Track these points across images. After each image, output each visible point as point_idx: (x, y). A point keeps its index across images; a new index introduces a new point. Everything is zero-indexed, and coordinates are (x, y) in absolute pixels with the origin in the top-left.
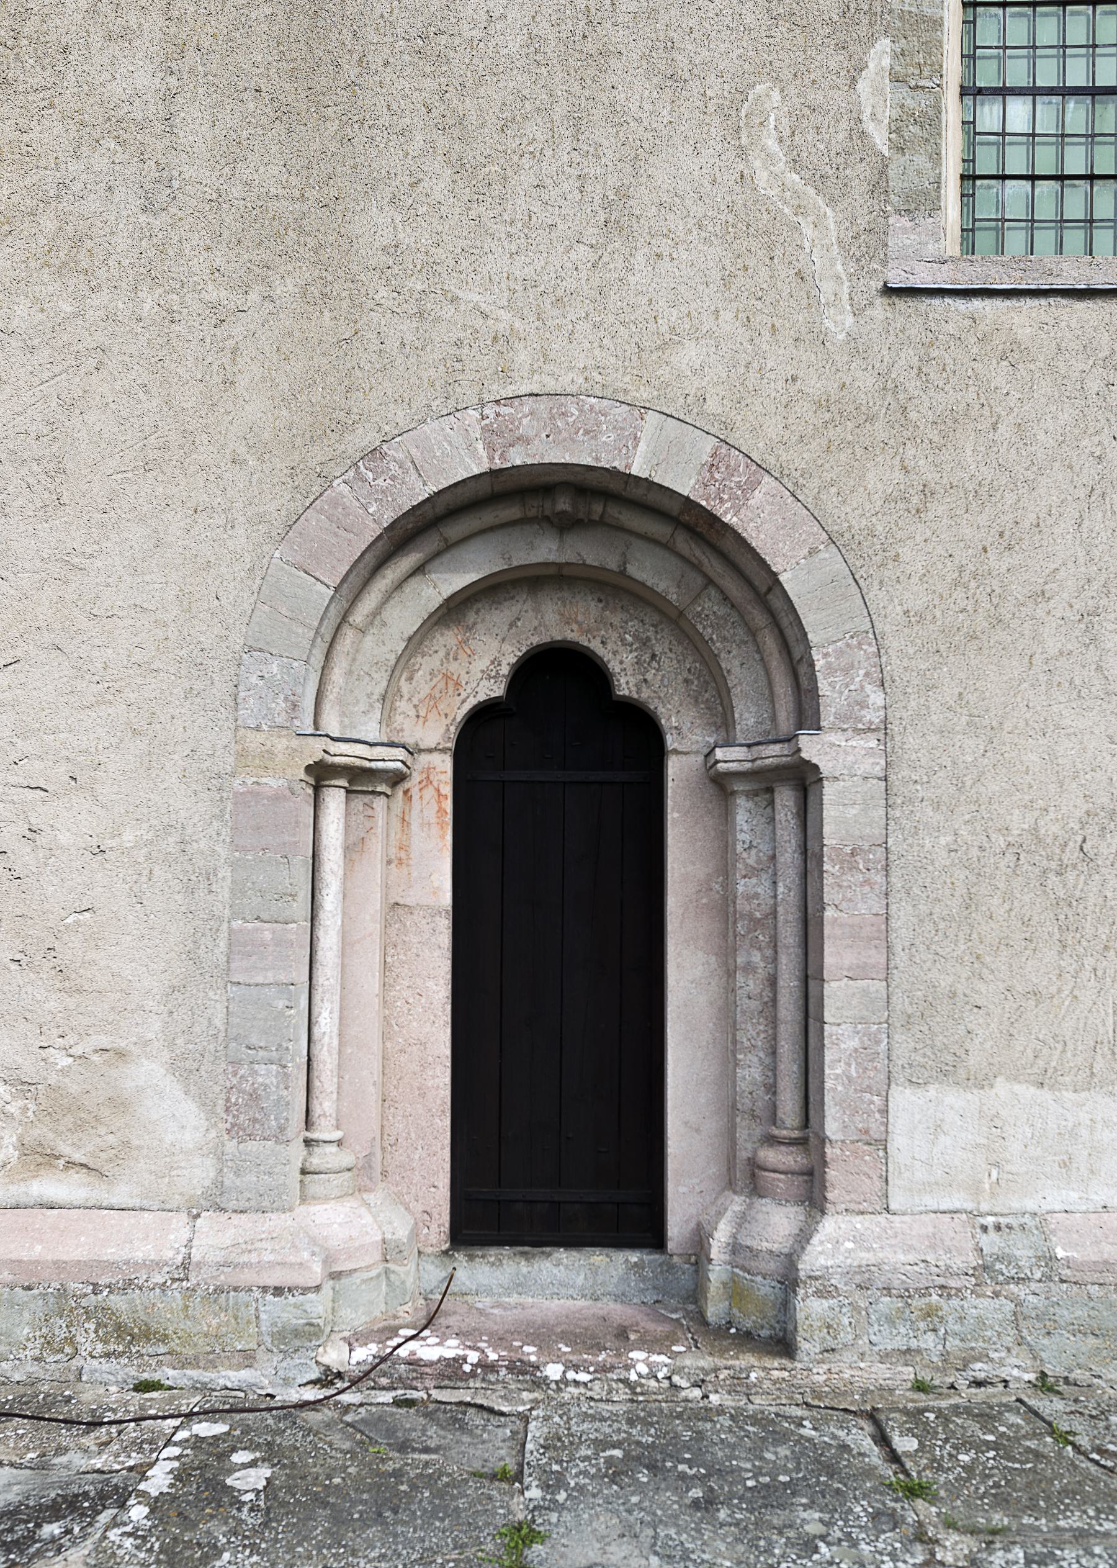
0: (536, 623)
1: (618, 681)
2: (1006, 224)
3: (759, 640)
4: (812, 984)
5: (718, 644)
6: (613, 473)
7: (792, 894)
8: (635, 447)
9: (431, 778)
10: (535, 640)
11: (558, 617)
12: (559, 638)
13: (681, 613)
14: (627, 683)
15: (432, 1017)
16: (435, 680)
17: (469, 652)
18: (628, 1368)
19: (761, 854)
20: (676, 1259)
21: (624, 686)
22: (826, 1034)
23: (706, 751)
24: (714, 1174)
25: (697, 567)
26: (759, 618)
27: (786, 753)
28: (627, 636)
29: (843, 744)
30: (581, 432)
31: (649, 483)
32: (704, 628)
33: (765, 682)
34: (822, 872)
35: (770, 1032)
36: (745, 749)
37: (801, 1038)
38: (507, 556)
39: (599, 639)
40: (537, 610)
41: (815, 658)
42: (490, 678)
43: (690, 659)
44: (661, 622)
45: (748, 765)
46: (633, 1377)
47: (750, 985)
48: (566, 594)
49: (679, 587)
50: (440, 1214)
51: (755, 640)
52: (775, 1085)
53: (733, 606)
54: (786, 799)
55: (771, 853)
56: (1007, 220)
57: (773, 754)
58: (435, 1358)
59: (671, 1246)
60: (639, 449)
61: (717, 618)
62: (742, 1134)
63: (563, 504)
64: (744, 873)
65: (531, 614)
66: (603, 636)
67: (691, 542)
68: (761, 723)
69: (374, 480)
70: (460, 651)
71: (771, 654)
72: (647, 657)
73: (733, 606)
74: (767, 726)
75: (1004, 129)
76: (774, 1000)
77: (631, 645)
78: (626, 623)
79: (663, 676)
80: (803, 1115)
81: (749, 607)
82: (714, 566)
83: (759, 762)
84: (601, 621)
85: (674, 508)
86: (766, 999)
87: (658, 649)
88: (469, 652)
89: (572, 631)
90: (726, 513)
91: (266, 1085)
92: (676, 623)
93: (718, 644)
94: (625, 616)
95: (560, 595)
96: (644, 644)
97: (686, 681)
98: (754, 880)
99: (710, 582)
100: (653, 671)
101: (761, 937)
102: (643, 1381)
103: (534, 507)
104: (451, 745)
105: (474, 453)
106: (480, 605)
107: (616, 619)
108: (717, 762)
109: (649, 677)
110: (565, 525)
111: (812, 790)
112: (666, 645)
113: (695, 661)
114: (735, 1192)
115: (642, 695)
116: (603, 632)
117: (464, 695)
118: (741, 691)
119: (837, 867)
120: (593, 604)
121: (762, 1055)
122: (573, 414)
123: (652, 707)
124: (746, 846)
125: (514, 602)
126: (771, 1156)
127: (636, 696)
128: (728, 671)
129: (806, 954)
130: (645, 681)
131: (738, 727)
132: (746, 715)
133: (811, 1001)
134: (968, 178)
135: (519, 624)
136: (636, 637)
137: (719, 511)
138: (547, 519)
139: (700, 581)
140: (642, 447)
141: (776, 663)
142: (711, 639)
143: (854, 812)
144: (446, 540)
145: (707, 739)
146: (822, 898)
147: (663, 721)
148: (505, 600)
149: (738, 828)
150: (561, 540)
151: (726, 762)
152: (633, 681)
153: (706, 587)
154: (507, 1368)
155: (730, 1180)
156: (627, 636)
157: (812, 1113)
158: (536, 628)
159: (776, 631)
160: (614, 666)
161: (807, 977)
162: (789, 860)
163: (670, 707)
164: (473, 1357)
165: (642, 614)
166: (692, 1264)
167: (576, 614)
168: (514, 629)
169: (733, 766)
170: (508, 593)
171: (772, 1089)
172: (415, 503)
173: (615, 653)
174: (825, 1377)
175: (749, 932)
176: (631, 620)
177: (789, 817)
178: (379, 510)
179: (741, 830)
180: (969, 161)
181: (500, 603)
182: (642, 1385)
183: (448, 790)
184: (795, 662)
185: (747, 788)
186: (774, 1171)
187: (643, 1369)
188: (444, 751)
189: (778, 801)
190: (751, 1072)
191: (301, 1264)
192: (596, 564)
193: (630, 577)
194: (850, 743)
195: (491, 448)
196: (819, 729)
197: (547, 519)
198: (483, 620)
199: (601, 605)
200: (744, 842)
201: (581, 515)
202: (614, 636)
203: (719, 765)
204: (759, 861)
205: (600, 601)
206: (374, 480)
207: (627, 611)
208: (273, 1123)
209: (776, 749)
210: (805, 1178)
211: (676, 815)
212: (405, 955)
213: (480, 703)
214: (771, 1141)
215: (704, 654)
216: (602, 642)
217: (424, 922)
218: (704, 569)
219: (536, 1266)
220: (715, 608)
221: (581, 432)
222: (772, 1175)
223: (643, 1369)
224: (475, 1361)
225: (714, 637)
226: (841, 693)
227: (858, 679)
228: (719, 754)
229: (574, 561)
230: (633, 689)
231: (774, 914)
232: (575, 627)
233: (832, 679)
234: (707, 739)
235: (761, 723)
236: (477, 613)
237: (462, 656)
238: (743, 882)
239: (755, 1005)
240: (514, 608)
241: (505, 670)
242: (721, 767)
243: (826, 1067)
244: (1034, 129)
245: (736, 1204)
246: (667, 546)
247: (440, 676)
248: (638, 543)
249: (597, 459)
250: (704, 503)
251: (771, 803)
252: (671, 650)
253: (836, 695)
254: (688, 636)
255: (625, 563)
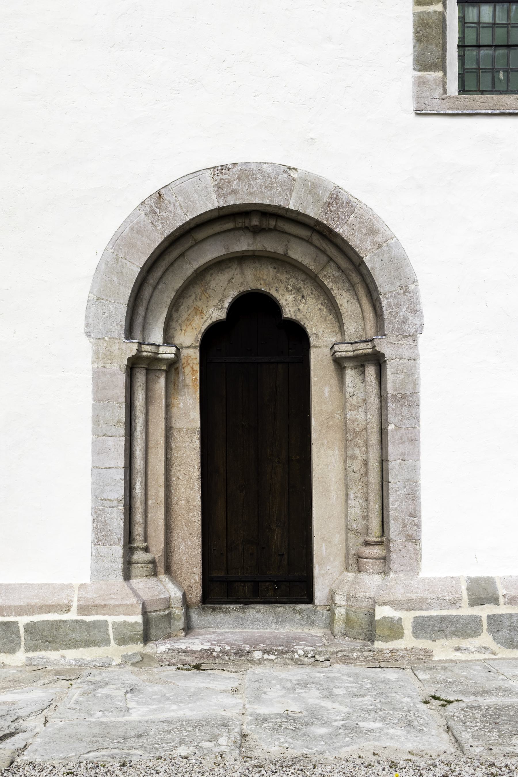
0: (242, 280)
1: (285, 310)
2: (481, 70)
3: (356, 289)
4: (384, 463)
5: (335, 291)
6: (279, 207)
7: (374, 418)
8: (291, 195)
9: (189, 361)
10: (242, 289)
11: (253, 277)
12: (254, 288)
13: (316, 276)
14: (290, 311)
15: (192, 486)
16: (190, 311)
17: (207, 296)
18: (294, 652)
19: (359, 399)
20: (318, 608)
21: (288, 312)
22: (390, 487)
23: (331, 345)
24: (186, 263)
25: (324, 252)
26: (355, 278)
27: (369, 347)
28: (289, 287)
29: (396, 343)
30: (264, 187)
31: (297, 213)
32: (328, 283)
33: (360, 310)
34: (387, 407)
35: (365, 489)
36: (350, 345)
37: (379, 492)
38: (226, 247)
39: (274, 288)
40: (242, 273)
41: (382, 300)
42: (218, 309)
43: (322, 298)
44: (306, 279)
45: (351, 354)
46: (296, 656)
47: (356, 465)
48: (257, 265)
49: (315, 262)
50: (197, 587)
51: (354, 289)
52: (367, 516)
53: (343, 271)
54: (371, 371)
55: (364, 398)
56: (482, 69)
57: (365, 348)
58: (199, 649)
59: (316, 601)
60: (293, 195)
61: (335, 277)
62: (351, 542)
63: (255, 221)
64: (350, 408)
65: (239, 276)
66: (277, 287)
67: (320, 240)
68: (358, 332)
69: (160, 213)
70: (203, 296)
71: (362, 296)
72: (299, 297)
73: (343, 271)
74: (361, 333)
75: (479, 21)
76: (366, 473)
77: (291, 291)
78: (289, 279)
79: (308, 307)
80: (381, 531)
81: (350, 273)
82: (332, 252)
83: (356, 352)
84: (275, 279)
85: (312, 224)
86: (362, 473)
87: (305, 293)
88: (207, 296)
89: (261, 284)
90: (336, 227)
91: (111, 518)
92: (315, 280)
93: (335, 291)
94: (288, 276)
95: (254, 265)
96: (298, 290)
97: (320, 309)
98: (355, 412)
99: (331, 259)
100: (303, 305)
101: (359, 441)
102: (301, 658)
103: (240, 222)
104: (198, 344)
105: (209, 198)
106: (212, 271)
107: (283, 277)
108: (335, 352)
109: (301, 307)
110: (256, 231)
111: (382, 365)
112: (309, 291)
113: (324, 299)
114: (348, 571)
115: (298, 317)
116: (276, 285)
117: (205, 318)
118: (348, 315)
119: (394, 404)
120: (271, 270)
121: (360, 501)
122: (259, 179)
123: (302, 323)
124: (351, 395)
125: (230, 269)
126: (368, 551)
127: (294, 318)
128: (341, 305)
129: (382, 449)
130: (299, 309)
131: (346, 334)
132: (350, 327)
133: (384, 472)
134: (461, 46)
135: (233, 281)
136: (294, 287)
137: (333, 226)
138: (247, 228)
139: (326, 259)
140: (294, 194)
141: (364, 300)
142: (332, 288)
143: (403, 377)
144: (195, 240)
145: (331, 339)
146: (387, 420)
147: (308, 331)
148: (226, 268)
149: (347, 385)
150: (254, 238)
151: (340, 352)
152: (292, 310)
153: (329, 262)
154: (235, 653)
155: (346, 567)
156: (289, 287)
157: (385, 529)
158: (242, 283)
159: (364, 285)
160: (282, 302)
161: (382, 460)
162: (372, 401)
163: (311, 323)
164: (218, 649)
165: (296, 275)
166: (327, 610)
167: (263, 275)
168: (230, 284)
169: (344, 354)
170: (227, 265)
171: (366, 518)
172: (181, 224)
173: (283, 295)
174: (390, 654)
175: (353, 438)
176: (291, 278)
177: (372, 379)
178: (163, 228)
179: (349, 387)
180: (462, 38)
181: (223, 270)
182: (300, 660)
183: (197, 368)
184: (374, 301)
185: (351, 365)
186: (367, 558)
187: (301, 652)
188: (194, 347)
189: (366, 371)
190: (356, 510)
191: (132, 605)
192: (272, 251)
193: (289, 257)
194: (400, 343)
195: (219, 196)
196: (385, 335)
197: (247, 228)
198: (214, 279)
199: (275, 271)
200: (350, 392)
201: (264, 226)
202: (282, 286)
203: (336, 354)
204: (358, 402)
205: (275, 268)
206: (160, 213)
207: (289, 274)
208: (115, 537)
209: (364, 345)
210: (382, 561)
211: (316, 379)
212: (177, 454)
213: (213, 322)
214: (367, 544)
215: (329, 296)
216: (276, 290)
217: (187, 436)
218: (327, 253)
219: (247, 613)
220: (334, 273)
221: (264, 187)
222: (365, 560)
223: (301, 652)
224: (219, 650)
225: (333, 287)
226: (395, 317)
227: (404, 310)
228: (336, 348)
229: (261, 249)
230: (293, 314)
231: (366, 429)
232: (262, 282)
233: (391, 310)
234: (331, 339)
235: (358, 332)
236: (211, 275)
237: (204, 298)
238: (350, 413)
239: (357, 476)
240: (230, 273)
241: (226, 305)
242: (338, 354)
243: (390, 504)
244: (495, 20)
245: (350, 576)
246: (308, 241)
247: (193, 309)
248: (293, 239)
249: (272, 201)
250: (325, 222)
251: (363, 373)
252: (312, 293)
253: (392, 318)
254: (321, 287)
255: (287, 250)
